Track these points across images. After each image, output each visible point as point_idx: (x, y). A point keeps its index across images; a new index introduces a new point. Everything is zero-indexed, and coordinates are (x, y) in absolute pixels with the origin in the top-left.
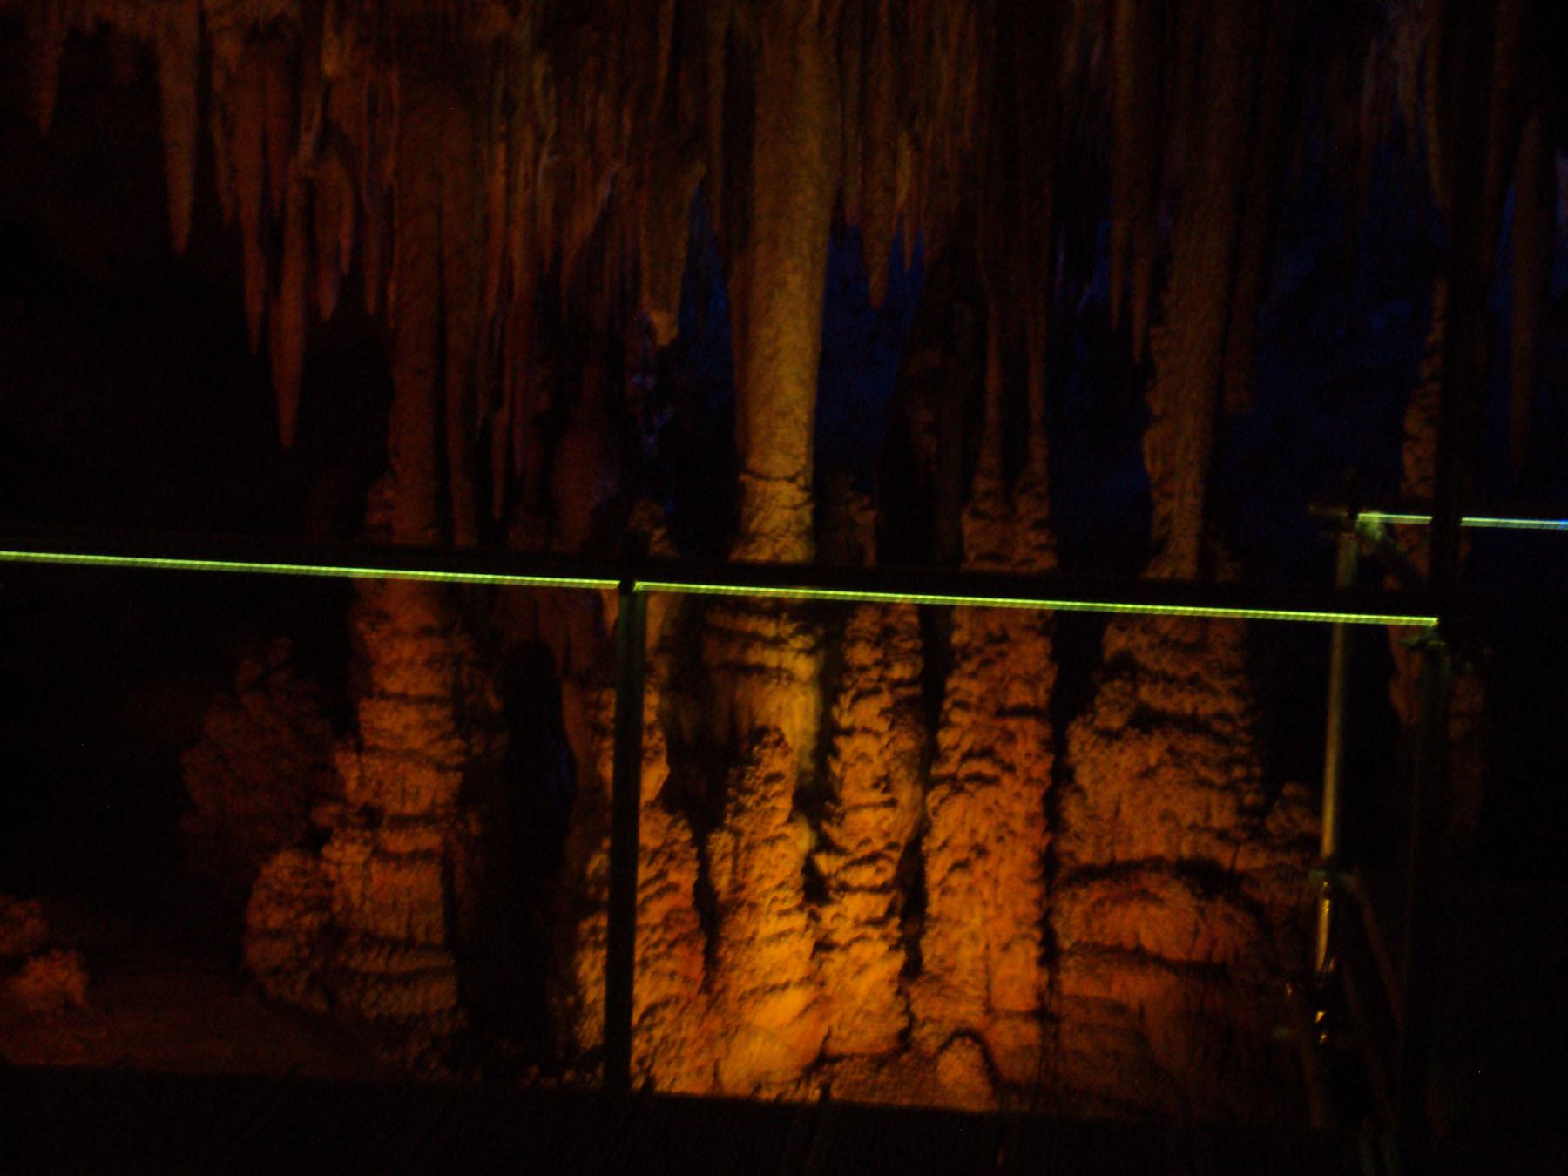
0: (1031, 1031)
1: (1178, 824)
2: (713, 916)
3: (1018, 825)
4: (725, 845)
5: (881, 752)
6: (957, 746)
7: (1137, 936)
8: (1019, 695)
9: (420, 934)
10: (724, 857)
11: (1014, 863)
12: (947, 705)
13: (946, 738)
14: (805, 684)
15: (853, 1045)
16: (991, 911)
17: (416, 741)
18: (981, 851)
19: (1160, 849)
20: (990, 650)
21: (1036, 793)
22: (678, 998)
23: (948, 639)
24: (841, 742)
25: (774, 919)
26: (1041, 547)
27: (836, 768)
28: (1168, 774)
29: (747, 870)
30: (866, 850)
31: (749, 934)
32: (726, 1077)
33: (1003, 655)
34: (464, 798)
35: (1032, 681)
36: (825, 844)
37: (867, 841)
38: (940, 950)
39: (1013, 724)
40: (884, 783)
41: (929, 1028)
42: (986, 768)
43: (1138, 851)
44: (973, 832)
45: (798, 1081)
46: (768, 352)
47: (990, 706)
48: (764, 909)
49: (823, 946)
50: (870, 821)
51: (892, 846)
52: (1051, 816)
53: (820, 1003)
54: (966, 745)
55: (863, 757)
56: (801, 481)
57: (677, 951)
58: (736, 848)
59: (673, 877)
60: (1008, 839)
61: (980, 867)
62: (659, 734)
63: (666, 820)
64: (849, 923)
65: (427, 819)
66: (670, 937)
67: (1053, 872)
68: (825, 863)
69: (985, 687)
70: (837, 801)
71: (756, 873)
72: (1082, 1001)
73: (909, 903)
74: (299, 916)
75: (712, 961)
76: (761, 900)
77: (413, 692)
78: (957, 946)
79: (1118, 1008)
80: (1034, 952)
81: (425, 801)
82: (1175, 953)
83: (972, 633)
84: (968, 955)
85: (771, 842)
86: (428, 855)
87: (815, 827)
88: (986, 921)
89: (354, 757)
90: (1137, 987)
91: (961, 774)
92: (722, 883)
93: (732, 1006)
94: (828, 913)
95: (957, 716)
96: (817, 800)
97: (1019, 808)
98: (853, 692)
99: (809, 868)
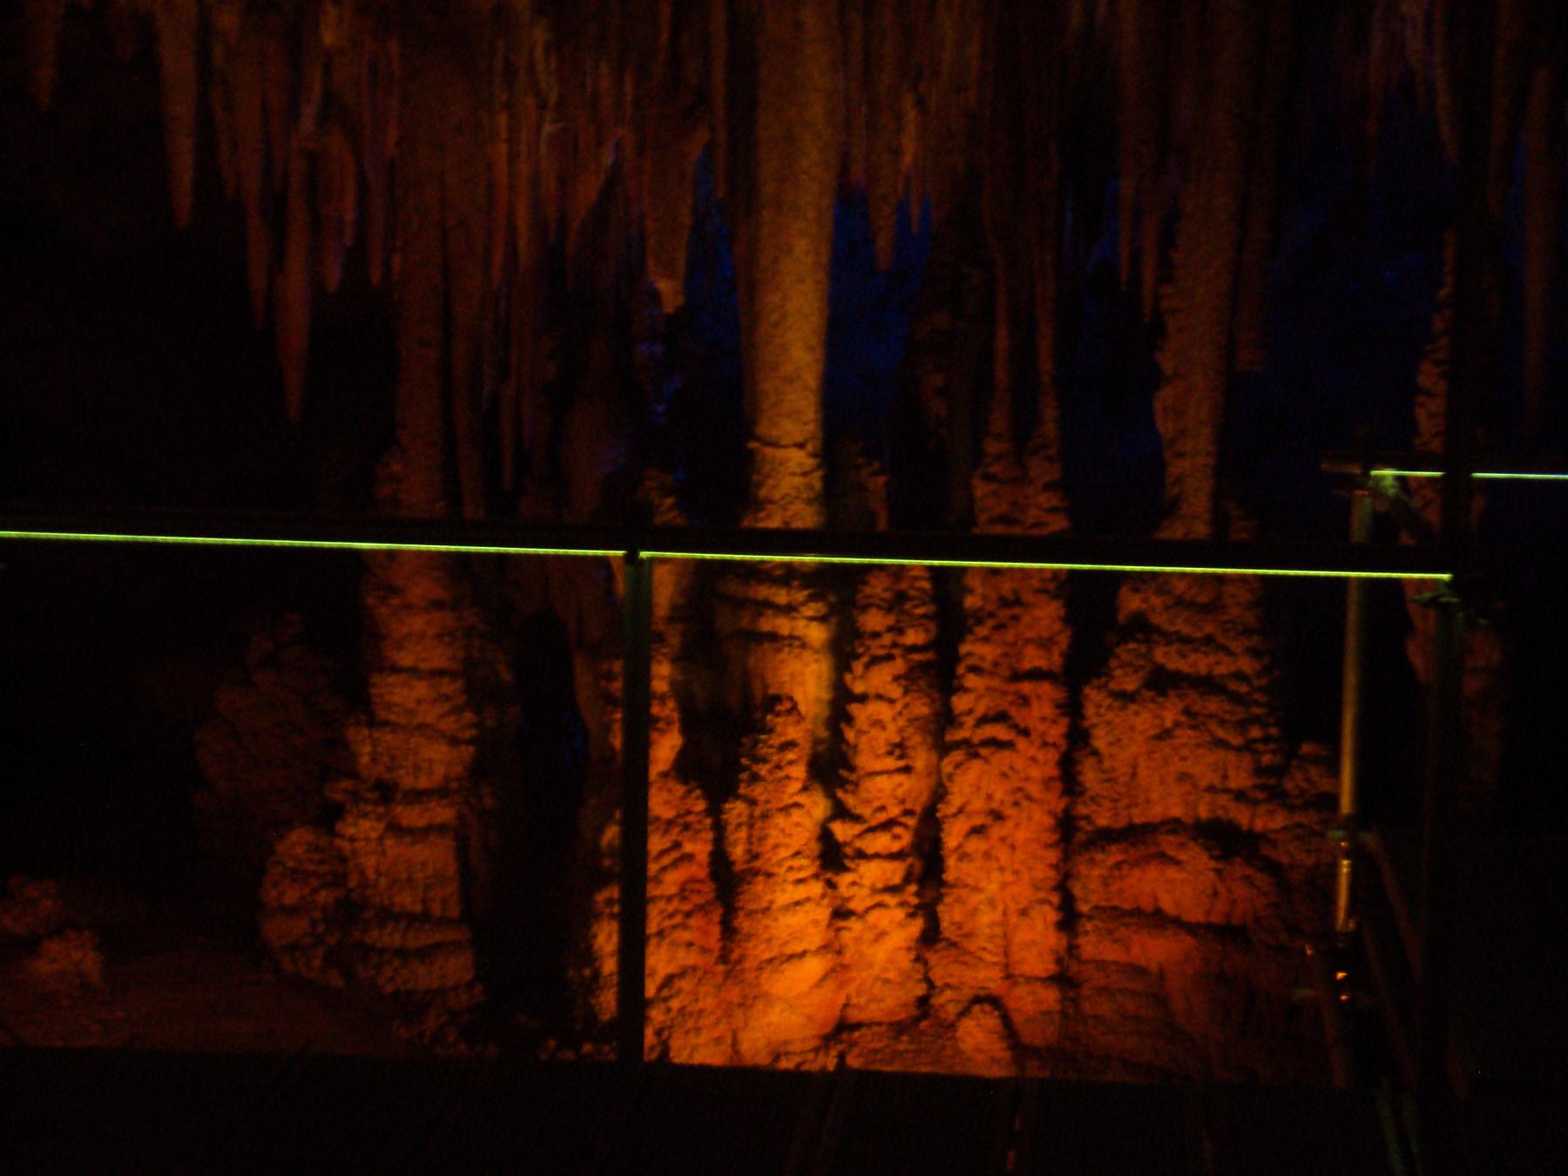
0: (1050, 996)
1: (1195, 786)
2: (728, 884)
3: (1034, 789)
4: (739, 815)
5: (894, 719)
6: (970, 711)
7: (1156, 899)
8: (1033, 659)
9: (436, 909)
10: (739, 825)
11: (1031, 827)
12: (961, 670)
13: (960, 703)
14: (816, 652)
15: (874, 1012)
16: (1008, 877)
17: (429, 714)
18: (998, 816)
19: (1177, 812)
20: (1004, 614)
21: (1052, 756)
22: (694, 968)
23: (960, 603)
24: (854, 708)
25: (790, 887)
26: (1052, 510)
27: (850, 735)
28: (1185, 736)
29: (762, 839)
30: (882, 817)
31: (764, 904)
32: (745, 1047)
33: (1015, 618)
34: (478, 771)
35: (1045, 644)
36: (841, 812)
37: (883, 808)
38: (957, 917)
39: (1026, 687)
40: (899, 748)
41: (948, 994)
42: (1000, 732)
43: (1156, 813)
44: (990, 797)
45: (816, 1050)
46: (775, 317)
47: (1005, 672)
48: (779, 879)
49: (841, 913)
50: (885, 788)
51: (908, 813)
52: (1068, 778)
53: (839, 971)
54: (981, 709)
55: (878, 724)
56: (810, 447)
57: (692, 922)
58: (751, 816)
59: (688, 847)
60: (1025, 803)
61: (997, 831)
62: (671, 704)
63: (680, 789)
64: (866, 891)
65: (441, 793)
66: (687, 907)
67: (1066, 827)
68: (841, 831)
69: (999, 651)
70: (852, 769)
71: (771, 841)
72: (1101, 965)
73: (927, 868)
74: (314, 891)
75: (729, 931)
76: (775, 870)
77: (423, 666)
78: (975, 911)
79: (1138, 971)
80: (1053, 916)
81: (440, 771)
82: (1195, 915)
83: (984, 598)
84: (986, 918)
85: (785, 810)
86: (442, 829)
87: (831, 795)
88: (1004, 886)
89: (366, 732)
90: (1156, 950)
91: (976, 740)
92: (738, 852)
93: (750, 976)
94: (844, 880)
95: (971, 681)
96: (831, 767)
97: (1035, 772)
98: (865, 659)
99: (825, 836)
